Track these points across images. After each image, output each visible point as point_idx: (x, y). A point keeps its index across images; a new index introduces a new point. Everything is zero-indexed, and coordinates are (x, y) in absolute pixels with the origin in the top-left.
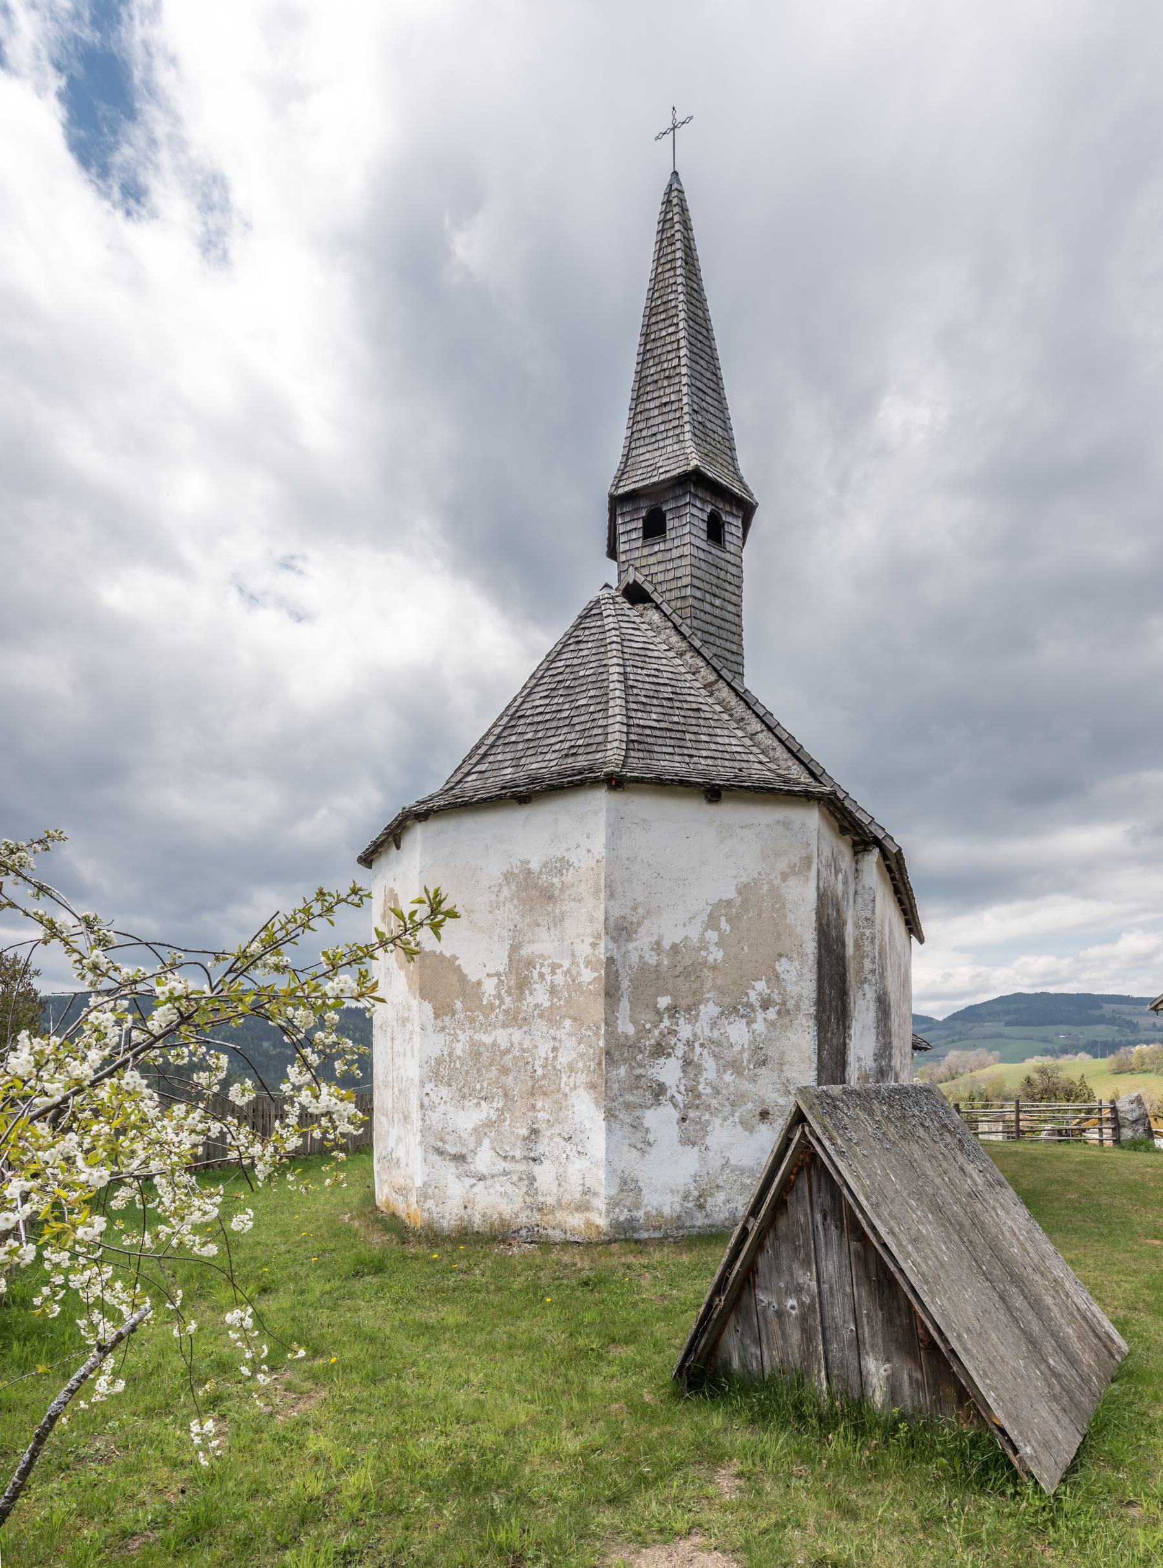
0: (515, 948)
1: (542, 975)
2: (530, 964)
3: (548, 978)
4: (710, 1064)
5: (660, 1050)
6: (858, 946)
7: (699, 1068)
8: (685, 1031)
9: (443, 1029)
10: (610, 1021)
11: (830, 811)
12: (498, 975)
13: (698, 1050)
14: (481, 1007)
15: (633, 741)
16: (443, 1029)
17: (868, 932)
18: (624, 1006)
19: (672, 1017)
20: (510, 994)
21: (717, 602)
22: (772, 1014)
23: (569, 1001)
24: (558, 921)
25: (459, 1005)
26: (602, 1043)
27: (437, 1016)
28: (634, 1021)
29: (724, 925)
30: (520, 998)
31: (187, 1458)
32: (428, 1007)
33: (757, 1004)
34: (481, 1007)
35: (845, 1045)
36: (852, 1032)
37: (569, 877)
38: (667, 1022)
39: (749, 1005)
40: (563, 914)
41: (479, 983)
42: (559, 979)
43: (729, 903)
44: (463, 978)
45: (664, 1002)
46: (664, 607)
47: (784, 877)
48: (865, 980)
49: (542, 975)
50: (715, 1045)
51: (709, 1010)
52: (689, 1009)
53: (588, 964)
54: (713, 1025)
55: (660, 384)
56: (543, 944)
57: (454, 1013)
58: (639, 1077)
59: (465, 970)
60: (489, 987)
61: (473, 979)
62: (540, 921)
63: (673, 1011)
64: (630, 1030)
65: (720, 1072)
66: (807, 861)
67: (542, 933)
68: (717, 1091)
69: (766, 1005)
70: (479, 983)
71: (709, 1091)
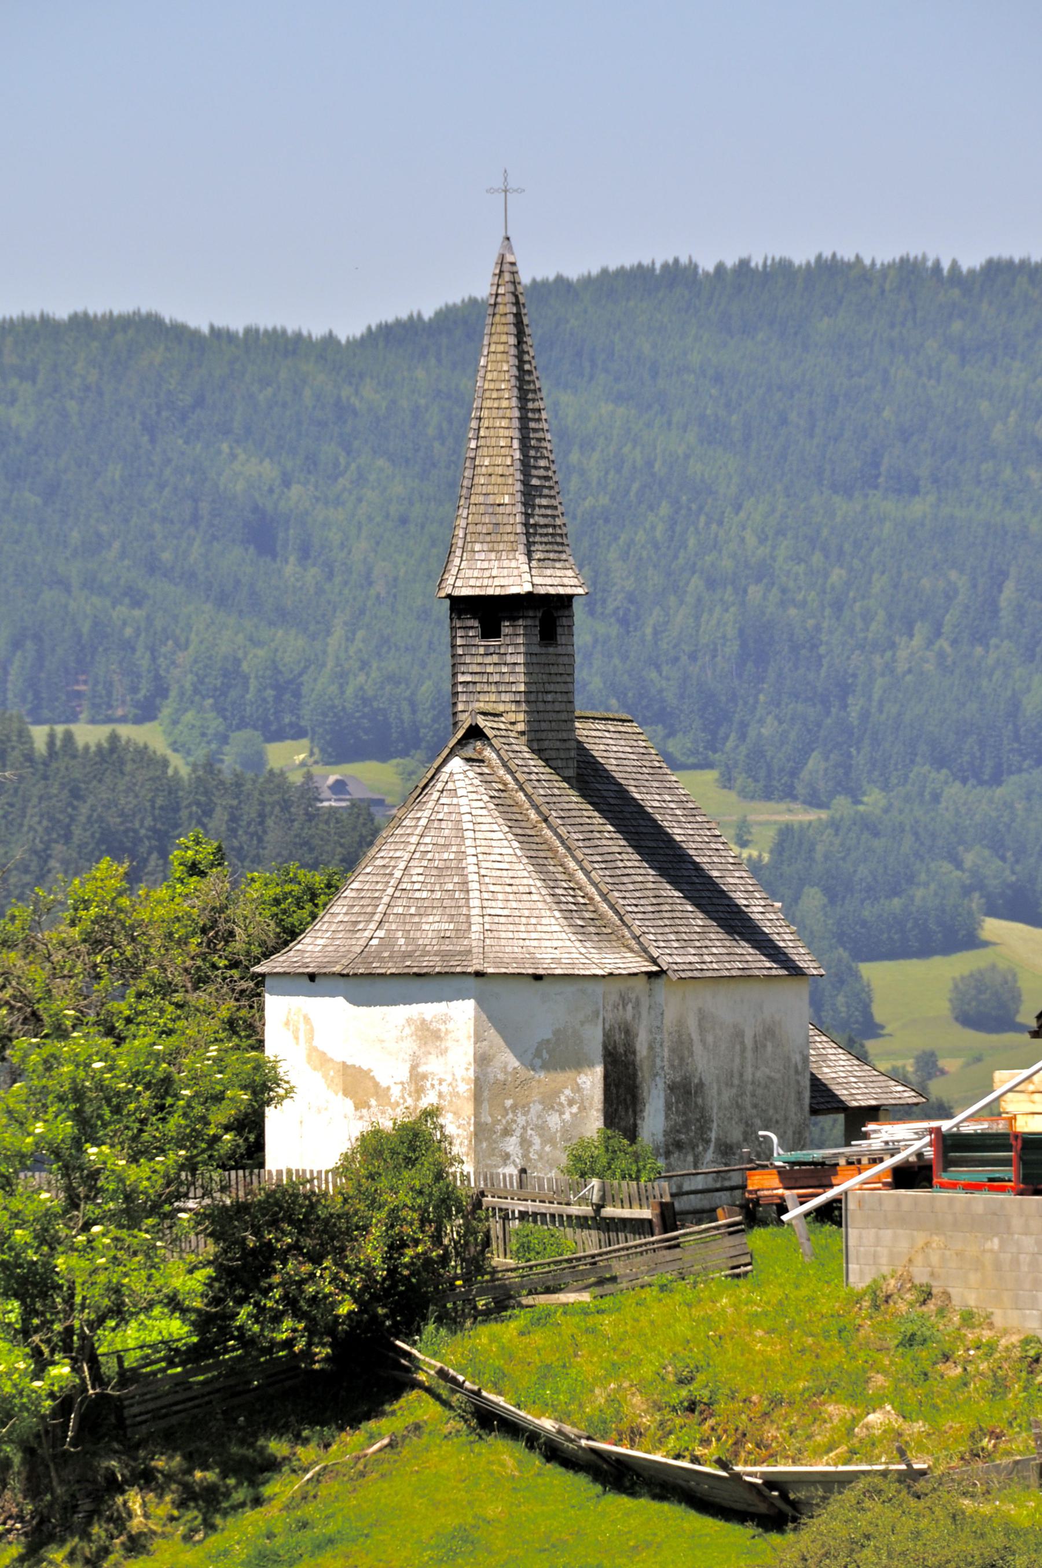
0: (414, 1068)
1: (433, 1086)
2: (424, 1077)
3: (437, 1087)
4: (537, 1140)
5: (507, 1132)
6: (651, 1048)
7: (530, 1144)
8: (521, 1120)
9: (361, 1118)
10: (477, 1115)
11: (496, 1319)
12: (402, 1083)
13: (530, 1132)
14: (389, 1104)
15: (535, 525)
16: (361, 1118)
17: (658, 1037)
18: (486, 1105)
19: (514, 1112)
20: (410, 1096)
21: (549, 697)
22: (575, 1109)
23: (450, 1102)
24: (444, 1052)
25: (373, 1102)
26: (472, 1128)
27: (357, 1108)
28: (491, 1115)
29: (545, 1055)
30: (418, 1099)
31: (148, 804)
32: (349, 1104)
33: (565, 1103)
34: (389, 1104)
35: (635, 1125)
36: (645, 1114)
37: (450, 1026)
38: (511, 1116)
39: (561, 1104)
40: (446, 1049)
41: (388, 1088)
42: (444, 1088)
43: (548, 1041)
44: (376, 1085)
45: (509, 1103)
46: (502, 752)
47: (582, 1024)
48: (656, 1074)
49: (433, 1086)
50: (542, 1129)
51: (536, 1108)
52: (523, 1107)
53: (463, 1080)
54: (539, 1117)
55: (493, 479)
56: (432, 1065)
57: (369, 1107)
58: (494, 1149)
59: (378, 1079)
60: (396, 1092)
61: (384, 1084)
62: (432, 1051)
63: (514, 1107)
64: (489, 1120)
65: (543, 1144)
66: (596, 1013)
67: (432, 1058)
68: (541, 1158)
69: (571, 1103)
70: (388, 1088)
71: (536, 1157)
